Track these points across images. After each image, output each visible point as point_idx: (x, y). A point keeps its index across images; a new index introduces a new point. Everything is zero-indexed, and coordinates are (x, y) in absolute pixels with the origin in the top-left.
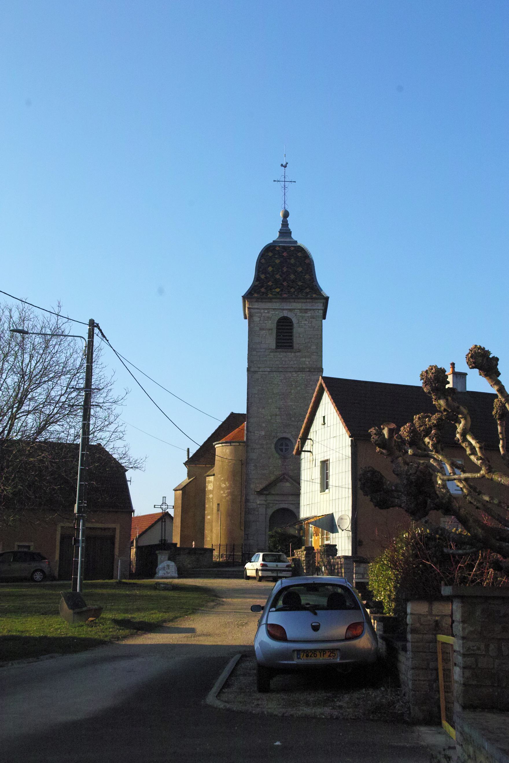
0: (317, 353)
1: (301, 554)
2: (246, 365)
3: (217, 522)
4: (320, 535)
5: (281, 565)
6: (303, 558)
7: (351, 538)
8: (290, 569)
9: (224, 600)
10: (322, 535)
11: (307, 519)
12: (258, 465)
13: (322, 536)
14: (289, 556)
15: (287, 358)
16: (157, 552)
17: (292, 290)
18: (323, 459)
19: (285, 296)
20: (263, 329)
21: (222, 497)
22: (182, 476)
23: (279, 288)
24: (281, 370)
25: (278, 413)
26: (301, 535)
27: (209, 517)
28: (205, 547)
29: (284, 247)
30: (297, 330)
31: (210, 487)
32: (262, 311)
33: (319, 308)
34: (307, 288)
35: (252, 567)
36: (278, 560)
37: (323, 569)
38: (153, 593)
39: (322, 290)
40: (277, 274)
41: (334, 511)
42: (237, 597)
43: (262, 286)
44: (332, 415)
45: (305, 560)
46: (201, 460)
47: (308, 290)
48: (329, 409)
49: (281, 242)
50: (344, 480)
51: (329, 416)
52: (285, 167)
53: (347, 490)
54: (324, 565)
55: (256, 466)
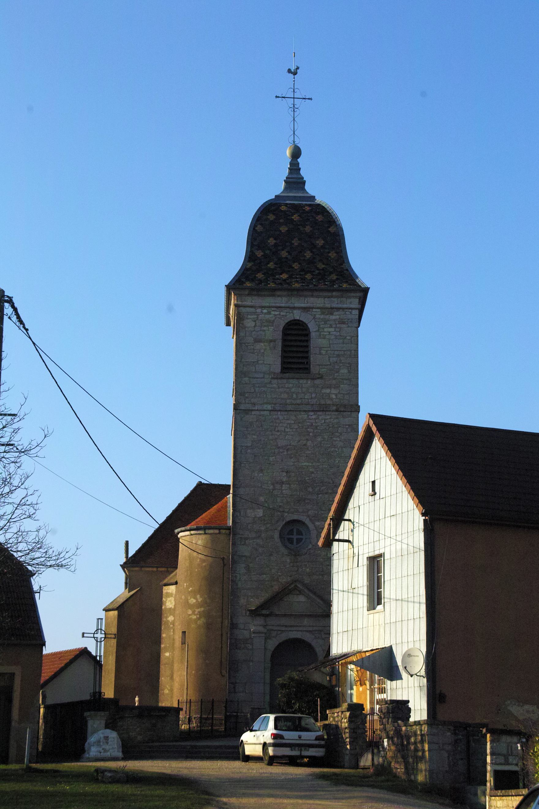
0: (349, 380)
1: (339, 717)
2: (231, 401)
3: (182, 662)
4: (368, 683)
5: (308, 737)
6: (345, 724)
7: (425, 689)
8: (323, 743)
9: (225, 800)
10: (372, 683)
11: (345, 656)
12: (251, 565)
13: (370, 686)
14: (316, 720)
15: (298, 388)
16: (86, 714)
17: (308, 276)
18: (371, 554)
19: (297, 285)
20: (260, 341)
21: (191, 619)
22: (115, 587)
23: (287, 272)
24: (289, 408)
25: (284, 479)
26: (334, 683)
27: (167, 654)
28: (160, 705)
29: (294, 206)
30: (317, 342)
31: (169, 603)
32: (259, 310)
33: (352, 306)
34: (331, 273)
35: (254, 741)
36: (297, 726)
37: (386, 744)
38: (90, 788)
39: (357, 277)
40: (283, 250)
41: (393, 643)
42: (244, 795)
43: (258, 271)
44: (388, 478)
45: (349, 727)
46: (152, 559)
47: (334, 277)
48: (383, 469)
49: (288, 198)
50: (411, 589)
51: (383, 481)
52: (295, 73)
53: (417, 605)
54: (388, 737)
55: (248, 568)
